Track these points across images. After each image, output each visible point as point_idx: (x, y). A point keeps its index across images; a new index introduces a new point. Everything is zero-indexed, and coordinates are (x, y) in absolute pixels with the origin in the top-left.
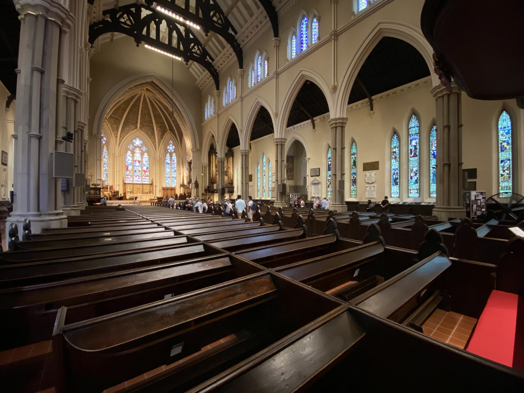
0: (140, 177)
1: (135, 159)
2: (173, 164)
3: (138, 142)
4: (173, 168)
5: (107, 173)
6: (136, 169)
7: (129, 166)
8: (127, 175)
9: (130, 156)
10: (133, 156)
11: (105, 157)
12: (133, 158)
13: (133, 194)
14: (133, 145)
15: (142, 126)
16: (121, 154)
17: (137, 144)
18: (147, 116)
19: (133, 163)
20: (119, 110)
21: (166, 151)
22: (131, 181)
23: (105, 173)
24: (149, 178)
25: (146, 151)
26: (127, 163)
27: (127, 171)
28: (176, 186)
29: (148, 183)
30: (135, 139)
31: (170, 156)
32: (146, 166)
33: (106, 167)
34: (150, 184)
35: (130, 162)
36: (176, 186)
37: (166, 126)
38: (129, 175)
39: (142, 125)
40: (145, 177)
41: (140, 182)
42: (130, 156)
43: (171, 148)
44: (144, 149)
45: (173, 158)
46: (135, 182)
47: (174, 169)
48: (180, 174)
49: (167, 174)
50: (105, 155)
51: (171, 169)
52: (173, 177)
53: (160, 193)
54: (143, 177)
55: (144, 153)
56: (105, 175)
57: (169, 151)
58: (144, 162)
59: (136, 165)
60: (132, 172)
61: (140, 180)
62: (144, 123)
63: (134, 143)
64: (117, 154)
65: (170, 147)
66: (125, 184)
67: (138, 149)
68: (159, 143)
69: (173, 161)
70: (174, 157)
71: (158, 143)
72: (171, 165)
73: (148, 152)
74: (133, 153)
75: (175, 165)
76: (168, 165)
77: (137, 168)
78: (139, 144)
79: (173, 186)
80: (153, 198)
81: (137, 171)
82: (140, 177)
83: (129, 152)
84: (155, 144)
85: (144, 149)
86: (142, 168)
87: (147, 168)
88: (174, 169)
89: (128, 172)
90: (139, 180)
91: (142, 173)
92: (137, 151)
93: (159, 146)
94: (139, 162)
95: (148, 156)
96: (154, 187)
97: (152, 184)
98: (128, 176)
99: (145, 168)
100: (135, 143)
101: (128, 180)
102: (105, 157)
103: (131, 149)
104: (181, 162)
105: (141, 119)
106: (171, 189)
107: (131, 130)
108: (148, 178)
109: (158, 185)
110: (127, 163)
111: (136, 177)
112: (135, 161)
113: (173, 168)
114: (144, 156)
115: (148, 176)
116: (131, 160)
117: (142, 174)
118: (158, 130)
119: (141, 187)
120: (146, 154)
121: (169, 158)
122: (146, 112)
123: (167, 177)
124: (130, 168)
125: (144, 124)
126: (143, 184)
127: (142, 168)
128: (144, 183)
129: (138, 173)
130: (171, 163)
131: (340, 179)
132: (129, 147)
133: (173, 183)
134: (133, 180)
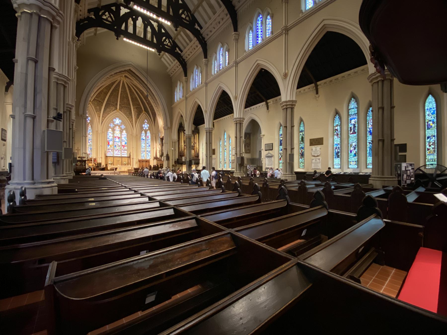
0: (120, 151)
1: (115, 135)
2: (147, 140)
3: (117, 121)
4: (148, 143)
5: (91, 147)
6: (116, 144)
7: (110, 142)
8: (108, 149)
9: (111, 133)
10: (113, 133)
11: (90, 133)
12: (113, 135)
13: (114, 165)
14: (114, 124)
15: (121, 107)
16: (104, 131)
17: (116, 122)
18: (125, 99)
19: (113, 139)
20: (102, 93)
21: (142, 128)
22: (112, 154)
23: (90, 147)
24: (127, 152)
25: (124, 129)
26: (108, 139)
27: (108, 146)
28: (150, 159)
29: (126, 156)
30: (116, 119)
31: (145, 133)
32: (125, 142)
33: (91, 143)
34: (128, 157)
35: (111, 138)
36: (150, 159)
37: (141, 107)
38: (110, 149)
39: (121, 106)
40: (124, 151)
41: (120, 156)
42: (111, 133)
43: (146, 126)
44: (123, 127)
45: (148, 135)
46: (115, 155)
47: (149, 144)
48: (154, 148)
49: (143, 148)
50: (90, 132)
51: (146, 144)
52: (148, 151)
53: (137, 165)
54: (122, 151)
55: (123, 130)
56: (89, 149)
57: (144, 129)
58: (123, 139)
59: (116, 140)
60: (112, 147)
61: (120, 153)
62: (123, 105)
63: (114, 122)
64: (99, 132)
65: (145, 125)
66: (106, 157)
67: (117, 127)
68: (136, 122)
69: (148, 137)
70: (149, 134)
71: (135, 122)
72: (146, 141)
73: (126, 129)
74: (113, 130)
75: (149, 141)
76: (144, 141)
77: (117, 143)
78: (118, 123)
79: (148, 159)
80: (130, 169)
81: (117, 146)
82: (120, 151)
83: (110, 130)
84: (132, 123)
85: (123, 127)
86: (121, 143)
87: (126, 143)
88: (149, 144)
89: (109, 147)
90: (118, 153)
91: (121, 147)
92: (117, 128)
93: (136, 124)
94: (119, 138)
95: (126, 133)
96: (132, 160)
97: (129, 157)
98: (109, 150)
99: (123, 143)
100: (115, 122)
101: (109, 153)
102: (89, 134)
103: (112, 127)
104: (154, 138)
105: (120, 102)
106: (146, 161)
107: (112, 111)
108: (126, 151)
109: (135, 157)
110: (108, 139)
111: (116, 151)
112: (116, 137)
113: (148, 143)
114: (123, 133)
115: (126, 150)
116: (112, 137)
117: (121, 148)
118: (135, 111)
119: (120, 159)
120: (124, 131)
121: (144, 134)
122: (125, 95)
123: (142, 151)
124: (111, 143)
125: (123, 106)
126: (122, 157)
127: (121, 143)
128: (123, 156)
129: (118, 148)
130: (146, 139)
131: (290, 153)
132: (110, 125)
133: (148, 156)
134: (114, 153)
